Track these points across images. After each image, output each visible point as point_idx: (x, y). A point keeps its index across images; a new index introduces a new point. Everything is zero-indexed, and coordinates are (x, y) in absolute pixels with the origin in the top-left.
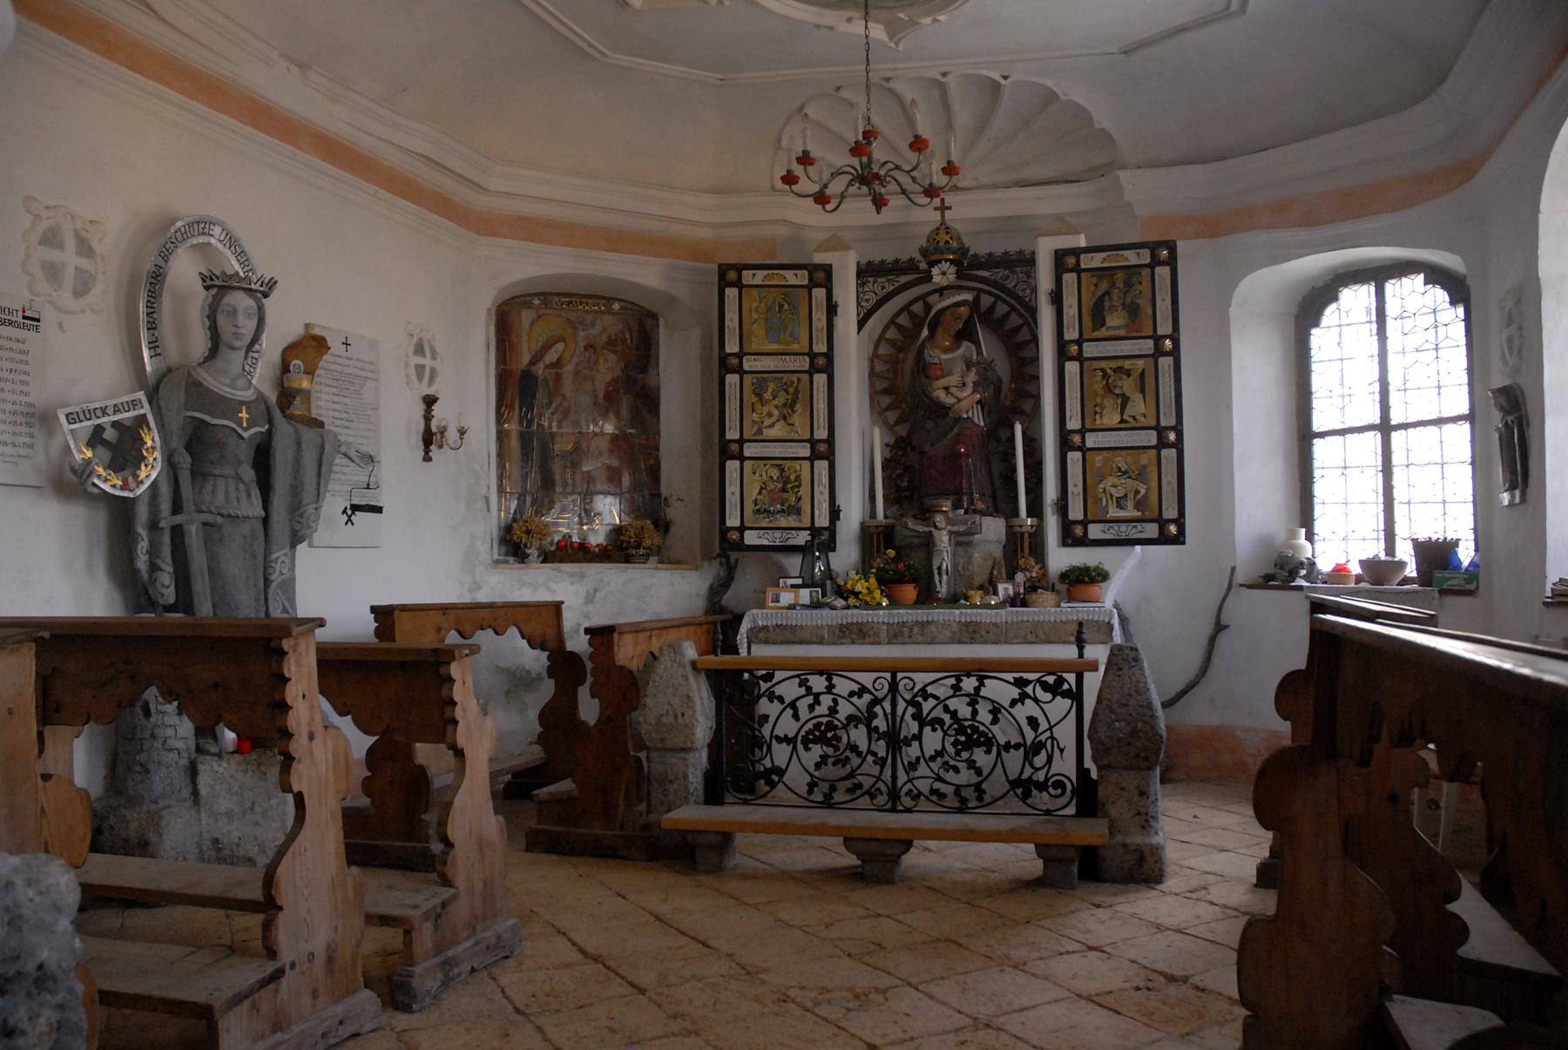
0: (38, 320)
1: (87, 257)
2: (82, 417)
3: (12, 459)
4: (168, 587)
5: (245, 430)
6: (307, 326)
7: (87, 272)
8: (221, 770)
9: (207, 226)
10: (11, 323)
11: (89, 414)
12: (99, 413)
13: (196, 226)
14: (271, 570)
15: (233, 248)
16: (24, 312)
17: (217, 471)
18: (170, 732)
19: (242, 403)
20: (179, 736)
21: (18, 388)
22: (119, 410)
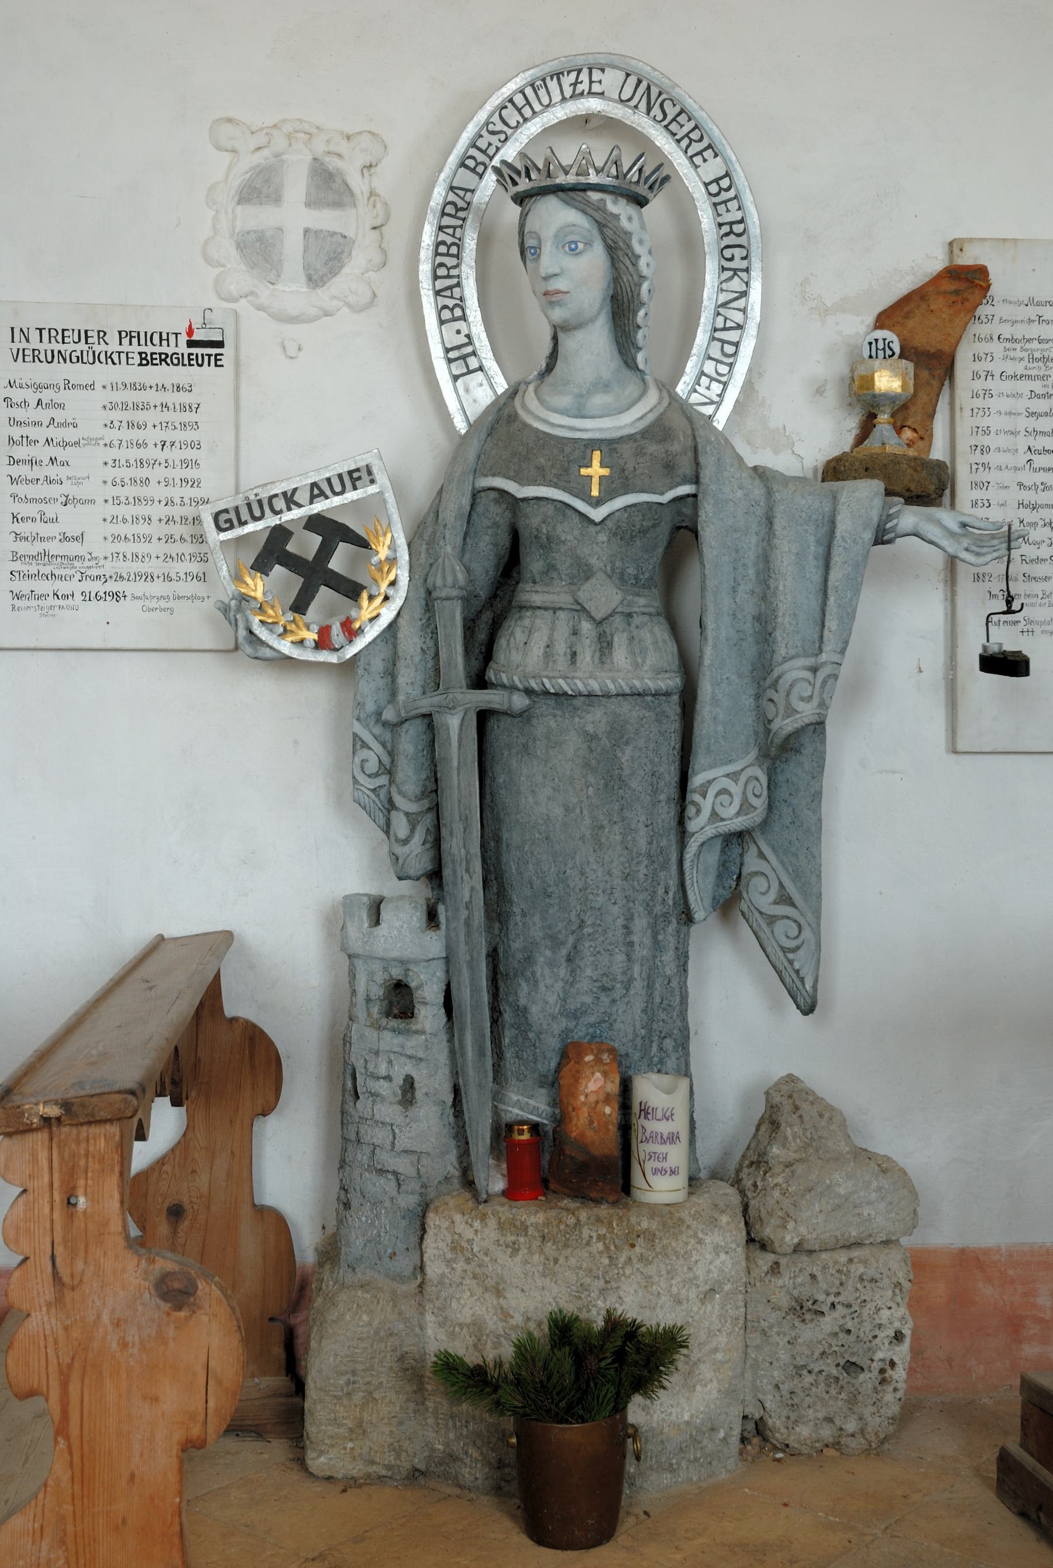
0: (220, 344)
1: (338, 205)
2: (245, 515)
3: (163, 604)
4: (405, 842)
5: (597, 503)
6: (951, 245)
7: (333, 234)
8: (469, 1234)
9: (584, 76)
10: (164, 358)
11: (256, 509)
12: (280, 504)
13: (553, 85)
14: (691, 811)
15: (656, 111)
16: (190, 332)
17: (537, 599)
18: (379, 1136)
19: (592, 444)
20: (398, 1147)
21: (179, 473)
22: (323, 494)
